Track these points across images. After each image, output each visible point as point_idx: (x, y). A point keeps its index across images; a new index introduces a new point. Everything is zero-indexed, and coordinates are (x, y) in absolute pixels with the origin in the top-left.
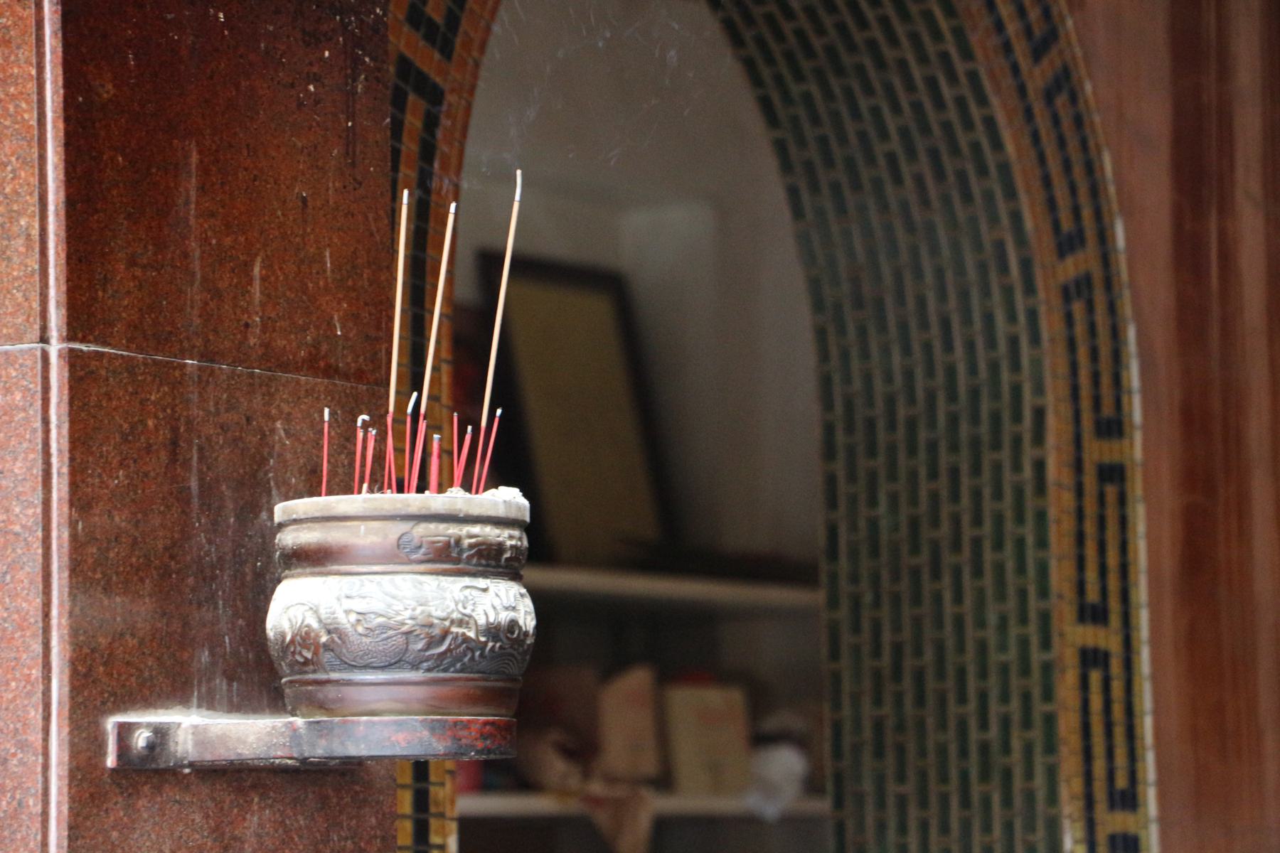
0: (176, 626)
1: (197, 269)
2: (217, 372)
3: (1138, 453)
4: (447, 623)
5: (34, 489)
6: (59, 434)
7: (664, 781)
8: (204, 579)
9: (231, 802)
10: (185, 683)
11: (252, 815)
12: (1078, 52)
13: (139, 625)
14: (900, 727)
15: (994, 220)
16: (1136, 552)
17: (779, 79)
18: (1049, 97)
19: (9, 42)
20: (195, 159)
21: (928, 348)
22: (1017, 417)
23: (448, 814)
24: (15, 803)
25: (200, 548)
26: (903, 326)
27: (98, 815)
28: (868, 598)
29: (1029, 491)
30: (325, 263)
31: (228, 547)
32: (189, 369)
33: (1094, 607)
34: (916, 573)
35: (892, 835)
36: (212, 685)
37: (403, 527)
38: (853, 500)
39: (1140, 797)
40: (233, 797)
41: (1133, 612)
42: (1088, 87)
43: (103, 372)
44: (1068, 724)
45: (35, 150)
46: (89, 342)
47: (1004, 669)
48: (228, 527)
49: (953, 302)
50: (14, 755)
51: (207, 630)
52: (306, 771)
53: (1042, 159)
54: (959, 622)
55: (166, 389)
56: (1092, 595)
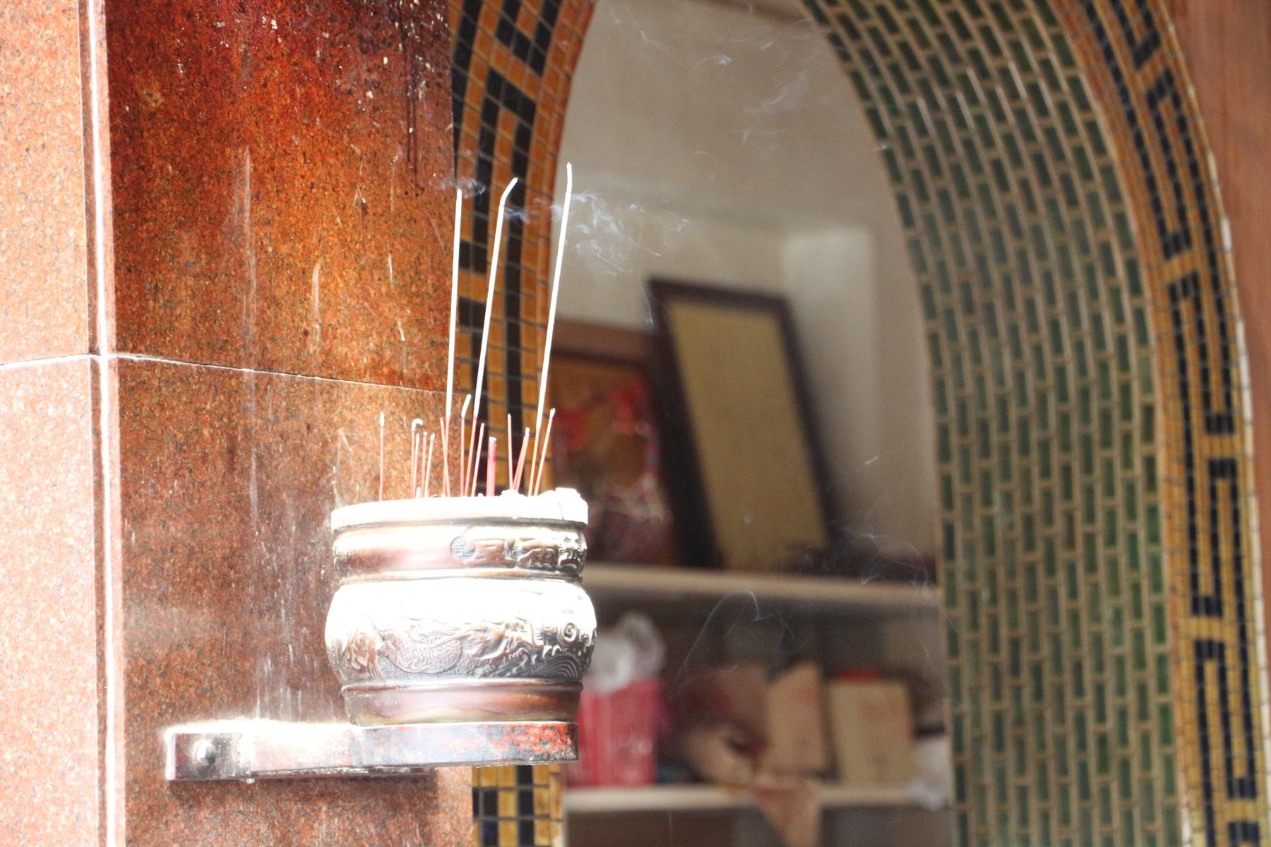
0: (237, 636)
1: (253, 278)
2: (275, 379)
3: (1249, 448)
4: (502, 628)
5: (86, 501)
6: (111, 445)
7: (830, 773)
8: (265, 588)
9: (298, 812)
10: (247, 693)
11: (320, 824)
12: (1181, 57)
13: (198, 636)
14: (1019, 721)
15: (1099, 221)
16: (1249, 543)
17: (885, 92)
18: (1152, 101)
19: (55, 52)
20: (248, 167)
21: (1038, 350)
22: (1127, 415)
23: (554, 815)
24: (73, 817)
25: (261, 557)
26: (1014, 330)
27: (157, 828)
28: (985, 595)
29: (1140, 487)
30: (386, 269)
31: (290, 556)
32: (246, 377)
33: (1207, 600)
34: (1031, 570)
35: (1013, 826)
36: (276, 694)
37: (460, 530)
38: (968, 499)
39: (1259, 785)
40: (299, 806)
41: (1247, 604)
42: (1191, 91)
43: (156, 382)
44: (1183, 715)
45: (82, 161)
46: (140, 352)
47: (1120, 661)
48: (290, 535)
49: (1061, 304)
50: (72, 769)
51: (269, 639)
52: (376, 779)
53: (1146, 162)
54: (1074, 617)
55: (222, 398)
56: (1206, 587)
